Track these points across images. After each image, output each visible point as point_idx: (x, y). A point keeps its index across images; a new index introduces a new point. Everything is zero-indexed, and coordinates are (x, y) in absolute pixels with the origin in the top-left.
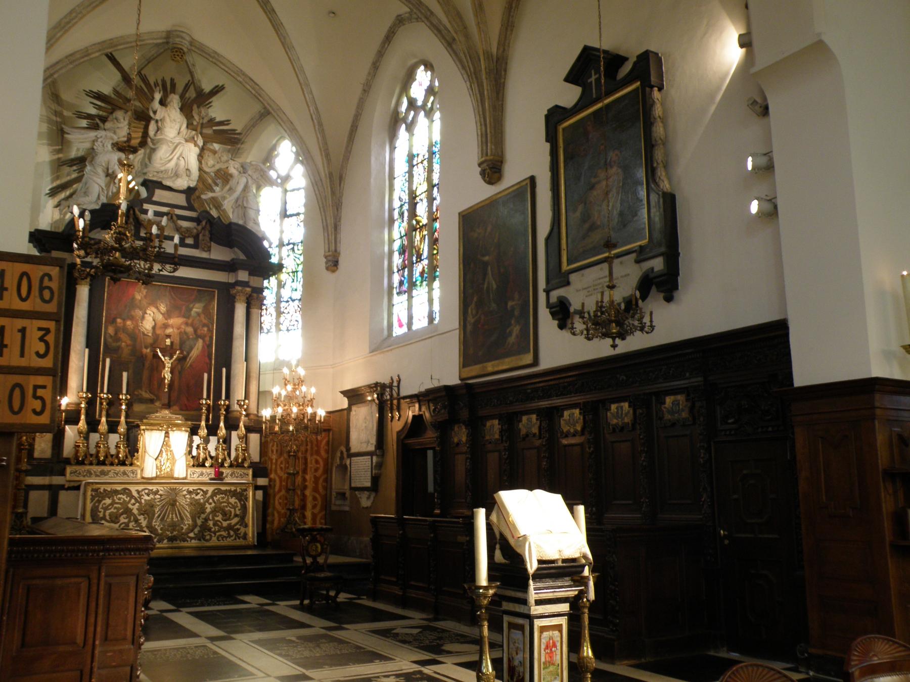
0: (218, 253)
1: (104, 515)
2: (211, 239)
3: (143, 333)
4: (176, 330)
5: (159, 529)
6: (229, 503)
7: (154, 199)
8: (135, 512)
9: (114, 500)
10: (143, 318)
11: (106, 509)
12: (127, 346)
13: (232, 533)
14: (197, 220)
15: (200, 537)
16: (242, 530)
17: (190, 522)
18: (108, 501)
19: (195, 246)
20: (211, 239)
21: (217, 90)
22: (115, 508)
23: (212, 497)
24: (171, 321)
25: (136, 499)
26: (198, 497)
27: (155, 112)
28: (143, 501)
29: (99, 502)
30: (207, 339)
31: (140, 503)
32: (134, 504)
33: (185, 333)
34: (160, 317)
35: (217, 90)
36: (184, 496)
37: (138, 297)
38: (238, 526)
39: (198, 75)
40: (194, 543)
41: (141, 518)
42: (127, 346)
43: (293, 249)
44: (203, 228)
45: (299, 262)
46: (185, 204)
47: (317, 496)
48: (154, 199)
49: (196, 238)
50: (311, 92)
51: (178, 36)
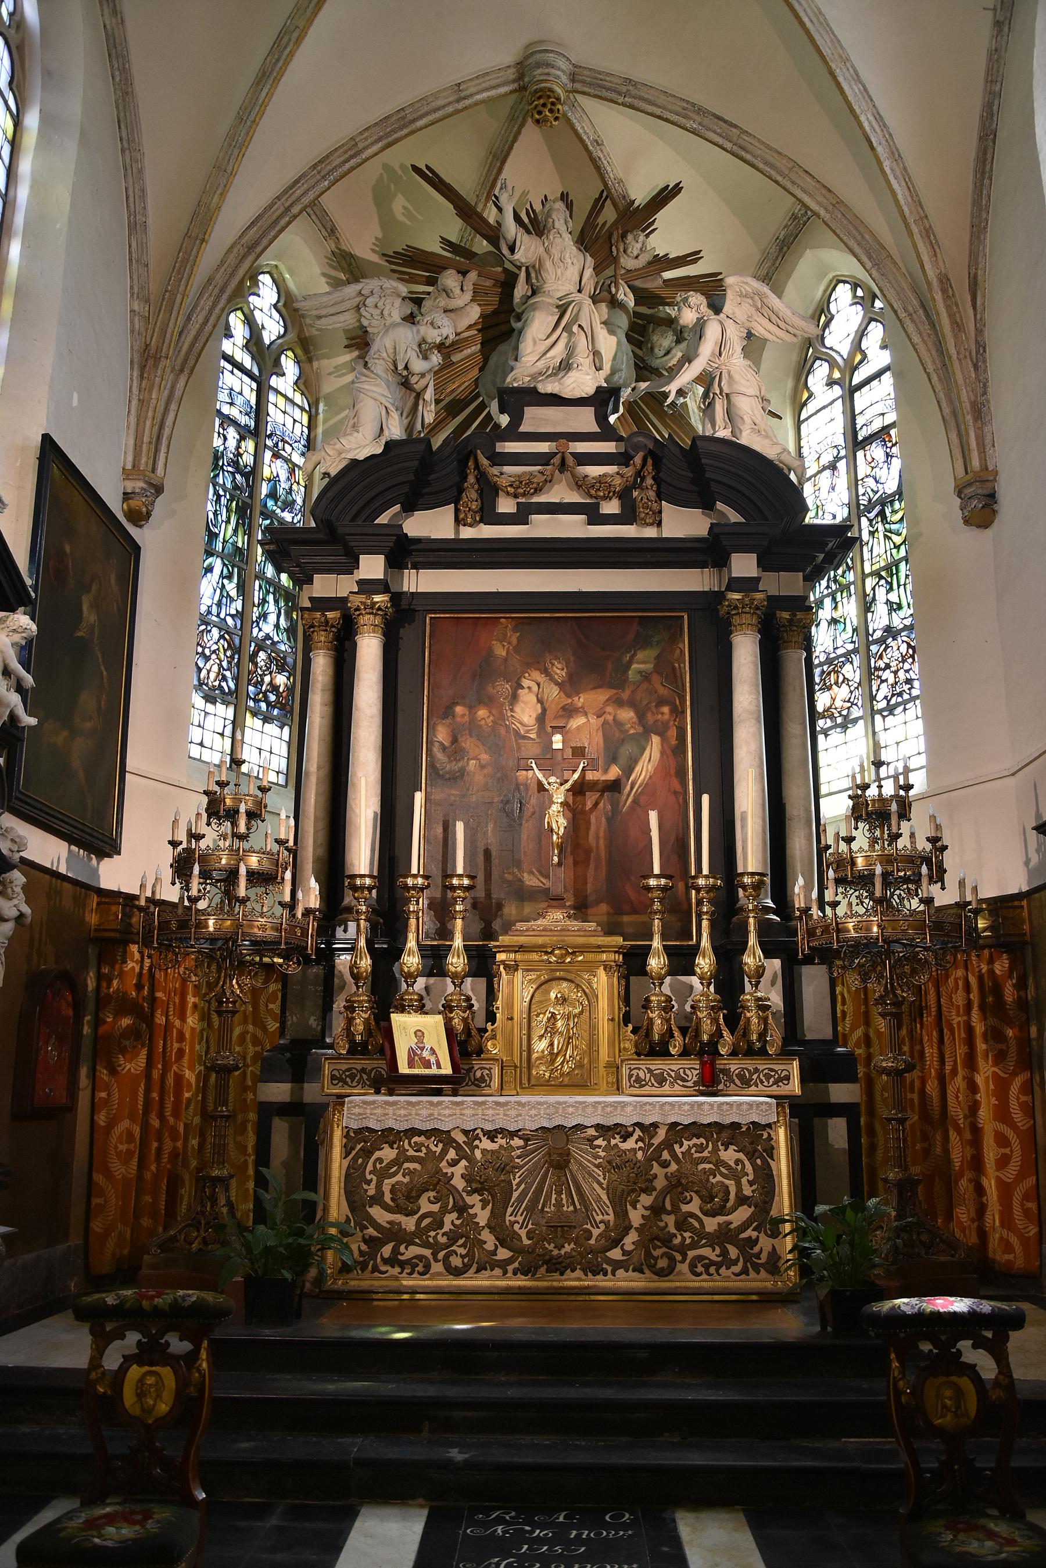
0: (682, 523)
1: (380, 1192)
2: (660, 497)
3: (517, 733)
4: (593, 719)
5: (523, 1233)
6: (719, 1163)
7: (522, 429)
8: (459, 1183)
9: (402, 1151)
10: (514, 698)
11: (383, 1174)
12: (482, 767)
13: (733, 1252)
14: (622, 459)
15: (657, 1250)
16: (765, 1243)
17: (611, 1218)
18: (388, 1153)
19: (627, 516)
20: (660, 497)
21: (665, 196)
22: (410, 1173)
23: (667, 1144)
24: (580, 700)
25: (458, 1148)
26: (630, 1144)
27: (512, 249)
28: (478, 1154)
29: (367, 1153)
30: (673, 732)
31: (471, 1159)
32: (454, 1163)
33: (617, 723)
34: (553, 692)
35: (665, 196)
36: (591, 1140)
37: (500, 651)
38: (750, 1233)
39: (616, 166)
40: (626, 1280)
41: (474, 1199)
42: (482, 767)
43: (882, 514)
44: (639, 474)
45: (898, 540)
46: (594, 428)
47: (1010, 1133)
48: (522, 429)
49: (624, 495)
50: (858, 79)
51: (538, 65)
